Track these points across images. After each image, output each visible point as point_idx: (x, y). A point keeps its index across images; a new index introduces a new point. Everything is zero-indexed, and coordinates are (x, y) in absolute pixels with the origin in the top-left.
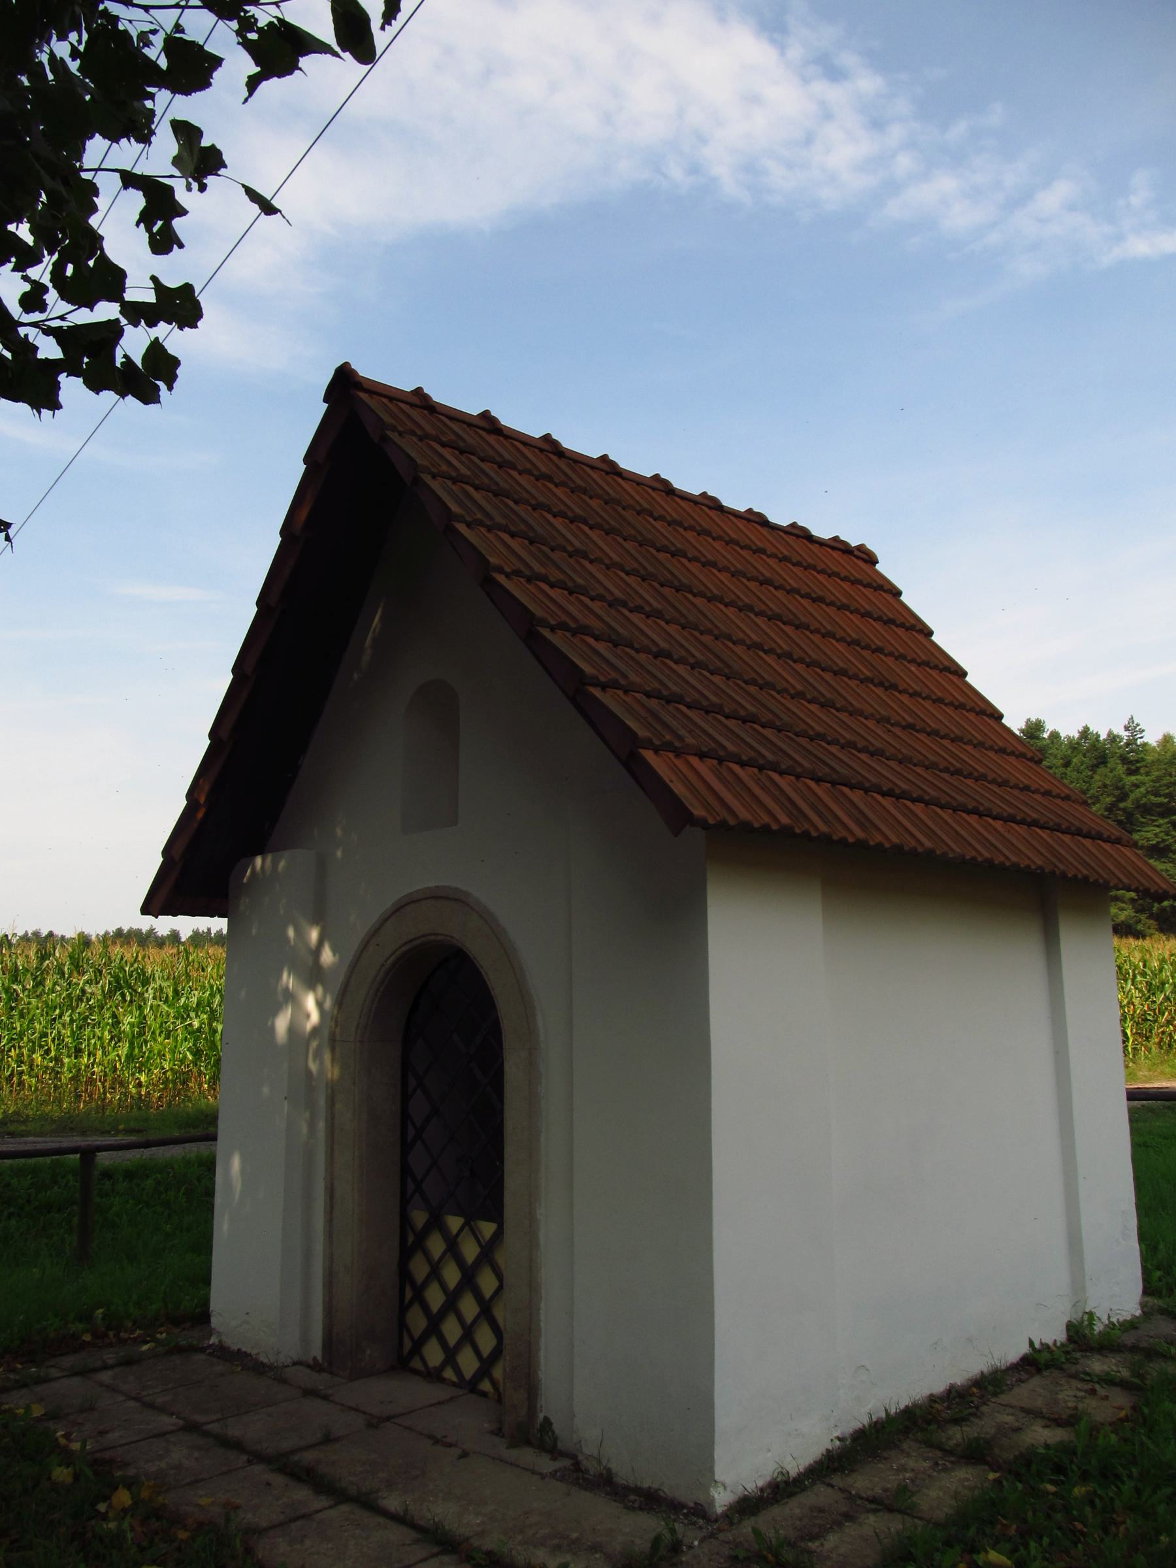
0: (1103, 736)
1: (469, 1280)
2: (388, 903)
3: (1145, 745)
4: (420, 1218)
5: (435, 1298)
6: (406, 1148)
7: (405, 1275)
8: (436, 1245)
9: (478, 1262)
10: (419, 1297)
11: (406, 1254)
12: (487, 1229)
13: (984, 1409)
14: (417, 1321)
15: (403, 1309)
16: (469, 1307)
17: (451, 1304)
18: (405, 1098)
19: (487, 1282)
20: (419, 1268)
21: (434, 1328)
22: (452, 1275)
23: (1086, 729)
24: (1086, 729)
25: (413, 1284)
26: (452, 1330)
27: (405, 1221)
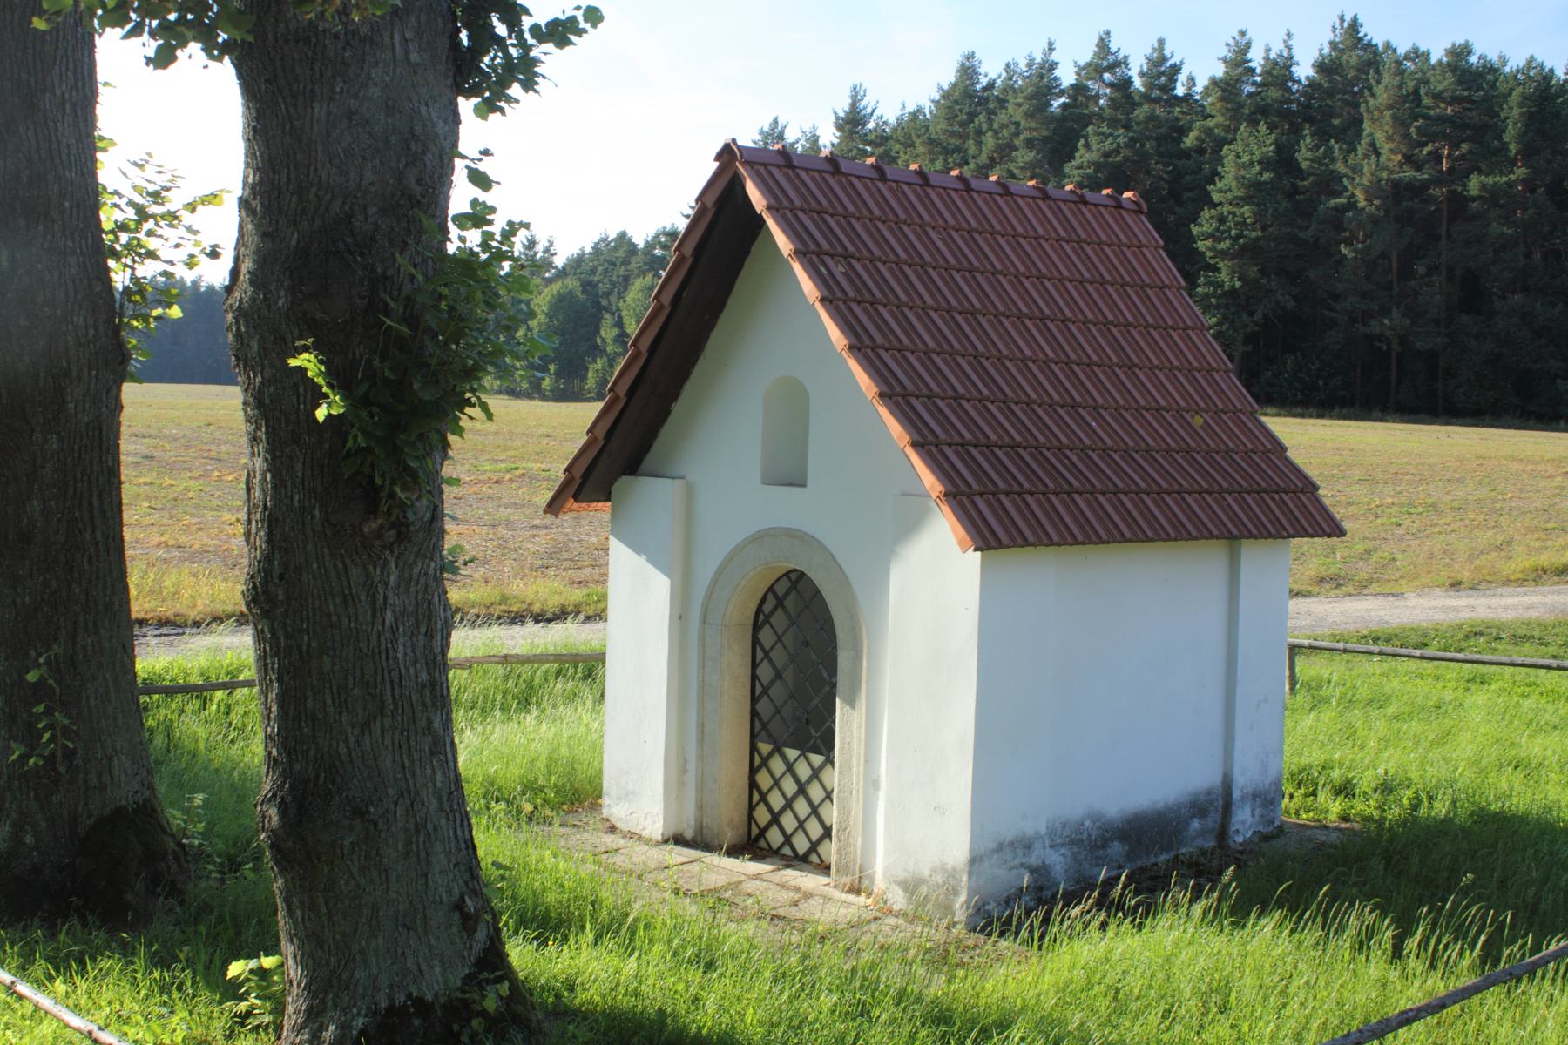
0: (1380, 47)
1: (802, 790)
2: (751, 529)
3: (991, 86)
4: (765, 748)
5: (776, 801)
6: (754, 699)
7: (753, 784)
8: (777, 765)
9: (809, 781)
10: (763, 798)
11: (753, 771)
12: (817, 759)
13: (1263, 127)
14: (762, 816)
15: (752, 808)
16: (802, 807)
17: (789, 804)
18: (754, 665)
19: (816, 792)
20: (764, 780)
21: (775, 819)
22: (790, 786)
23: (1532, 59)
24: (1532, 59)
25: (763, 648)
26: (788, 822)
27: (753, 749)
